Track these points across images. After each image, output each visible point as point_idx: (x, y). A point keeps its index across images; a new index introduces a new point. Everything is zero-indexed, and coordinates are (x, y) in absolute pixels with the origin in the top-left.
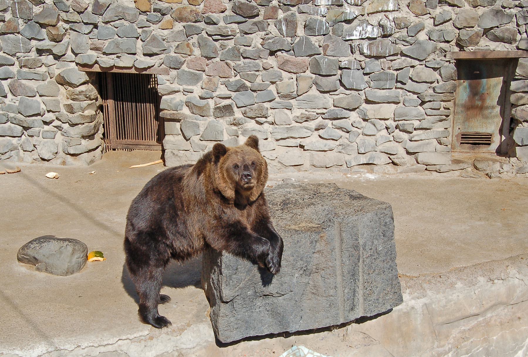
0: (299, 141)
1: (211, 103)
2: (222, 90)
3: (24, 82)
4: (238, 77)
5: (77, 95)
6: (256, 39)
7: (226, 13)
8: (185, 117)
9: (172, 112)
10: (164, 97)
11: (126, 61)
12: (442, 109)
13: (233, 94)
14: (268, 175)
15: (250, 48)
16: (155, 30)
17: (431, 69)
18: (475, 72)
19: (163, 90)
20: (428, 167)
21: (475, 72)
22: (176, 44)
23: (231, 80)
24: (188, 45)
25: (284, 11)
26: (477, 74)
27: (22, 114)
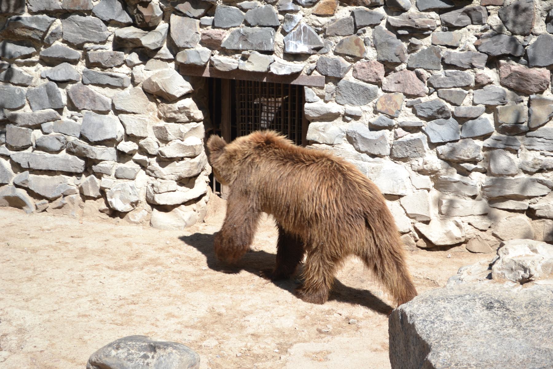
3: (91, 88)
15: (457, 51)
19: (313, 110)
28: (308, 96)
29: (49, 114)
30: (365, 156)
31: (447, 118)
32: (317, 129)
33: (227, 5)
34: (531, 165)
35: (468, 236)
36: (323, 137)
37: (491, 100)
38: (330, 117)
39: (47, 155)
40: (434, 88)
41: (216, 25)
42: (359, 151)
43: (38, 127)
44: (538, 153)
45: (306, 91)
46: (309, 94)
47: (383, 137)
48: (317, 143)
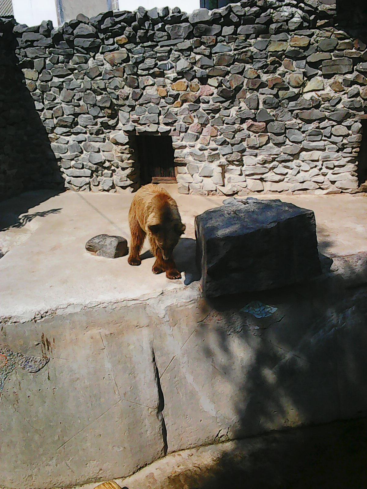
0: (259, 177)
1: (206, 153)
2: (213, 145)
3: (92, 143)
4: (222, 136)
5: (124, 150)
6: (233, 111)
7: (214, 96)
8: (190, 162)
9: (181, 159)
10: (176, 150)
11: (152, 128)
12: (353, 153)
13: (219, 147)
14: (142, 249)
15: (230, 118)
16: (174, 109)
17: (345, 127)
18: (337, 24)
19: (176, 145)
20: (344, 191)
21: (337, 24)
22: (183, 116)
23: (217, 138)
24: (190, 117)
25: (250, 93)
26: (336, 24)
27: (91, 163)
28: (173, 140)
29: (77, 154)
30: (197, 161)
31: (228, 144)
32: (178, 152)
33: (254, 149)
34: (261, 161)
35: (238, 190)
36: (180, 155)
37: (243, 136)
38: (183, 147)
39: (267, 174)
40: (91, 79)
41: (157, 122)
42: (194, 159)
43: (72, 160)
44: (264, 156)
45: (172, 138)
46: (174, 138)
47: (203, 153)
48: (178, 158)
